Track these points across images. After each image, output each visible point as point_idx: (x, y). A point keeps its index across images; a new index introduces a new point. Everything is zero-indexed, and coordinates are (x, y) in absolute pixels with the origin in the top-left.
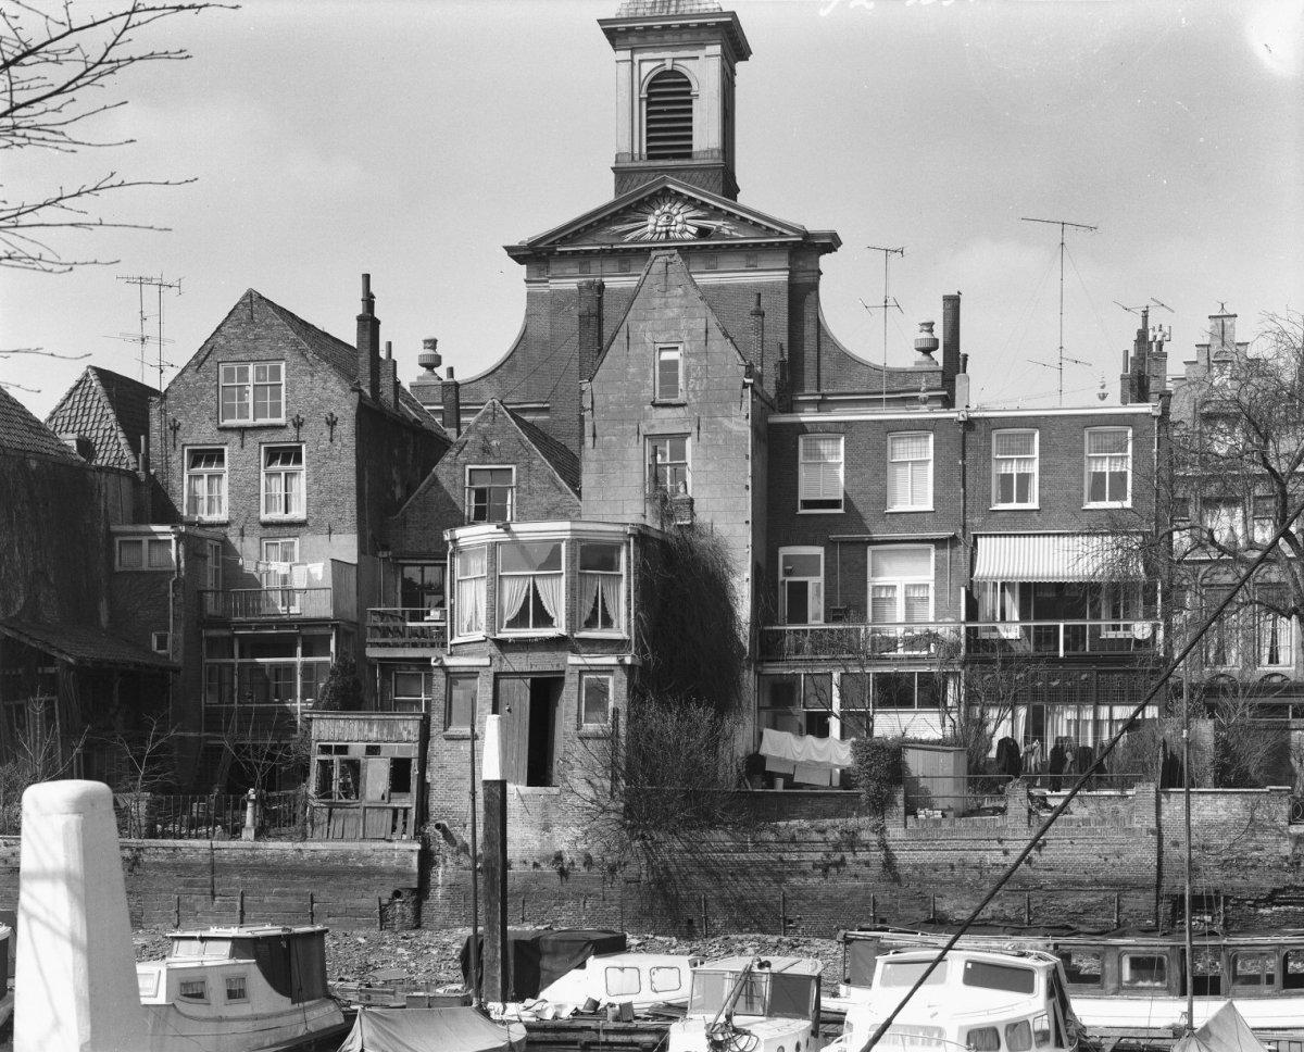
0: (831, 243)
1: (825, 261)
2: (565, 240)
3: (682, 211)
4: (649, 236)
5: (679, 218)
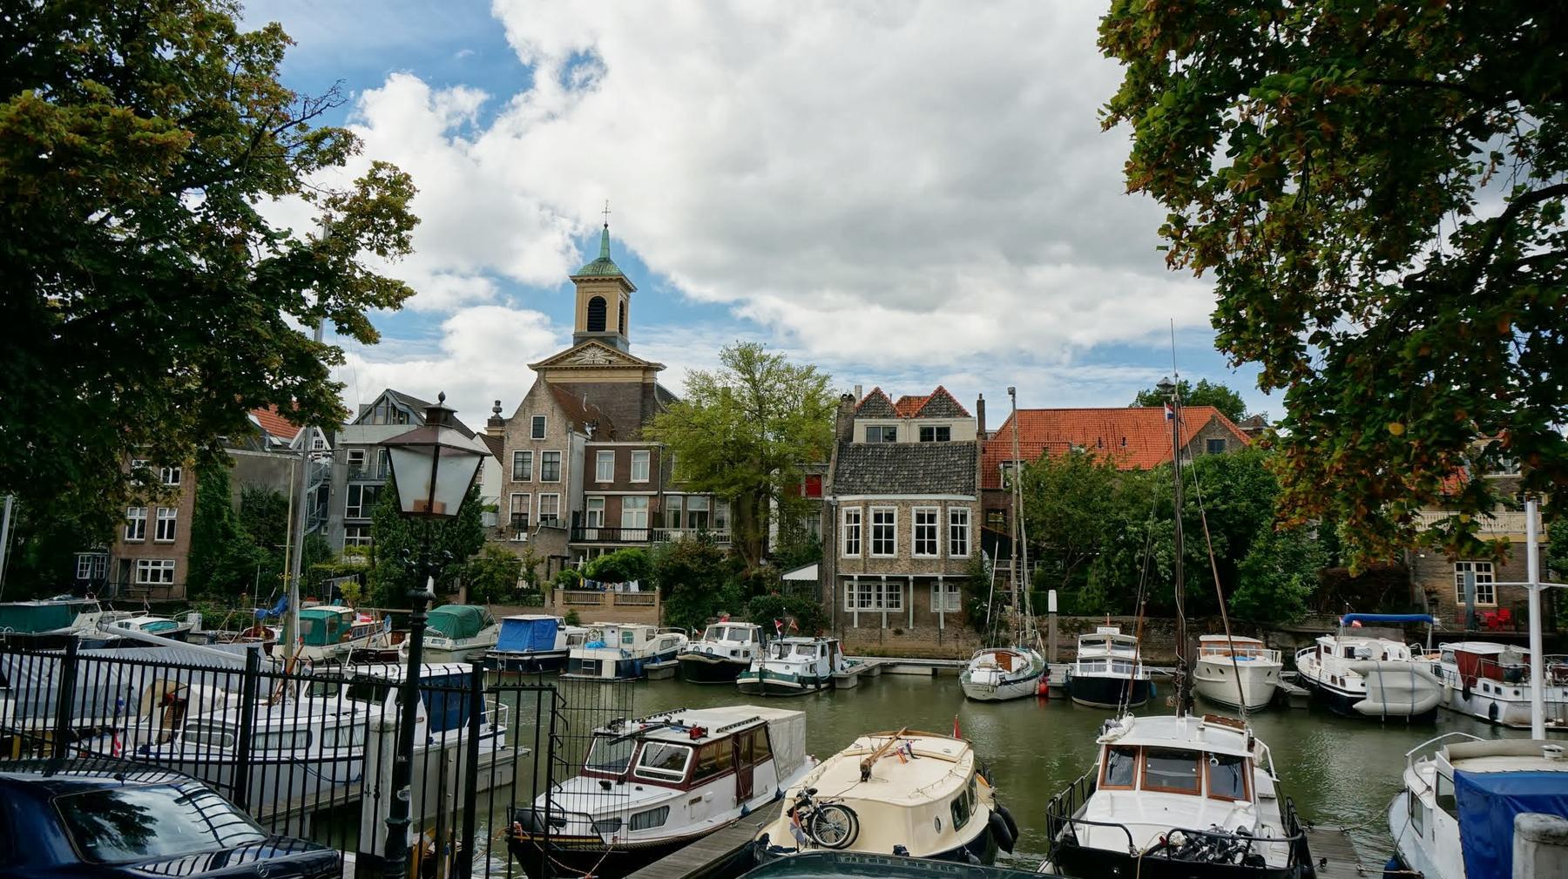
0: (658, 368)
1: (659, 374)
2: (552, 363)
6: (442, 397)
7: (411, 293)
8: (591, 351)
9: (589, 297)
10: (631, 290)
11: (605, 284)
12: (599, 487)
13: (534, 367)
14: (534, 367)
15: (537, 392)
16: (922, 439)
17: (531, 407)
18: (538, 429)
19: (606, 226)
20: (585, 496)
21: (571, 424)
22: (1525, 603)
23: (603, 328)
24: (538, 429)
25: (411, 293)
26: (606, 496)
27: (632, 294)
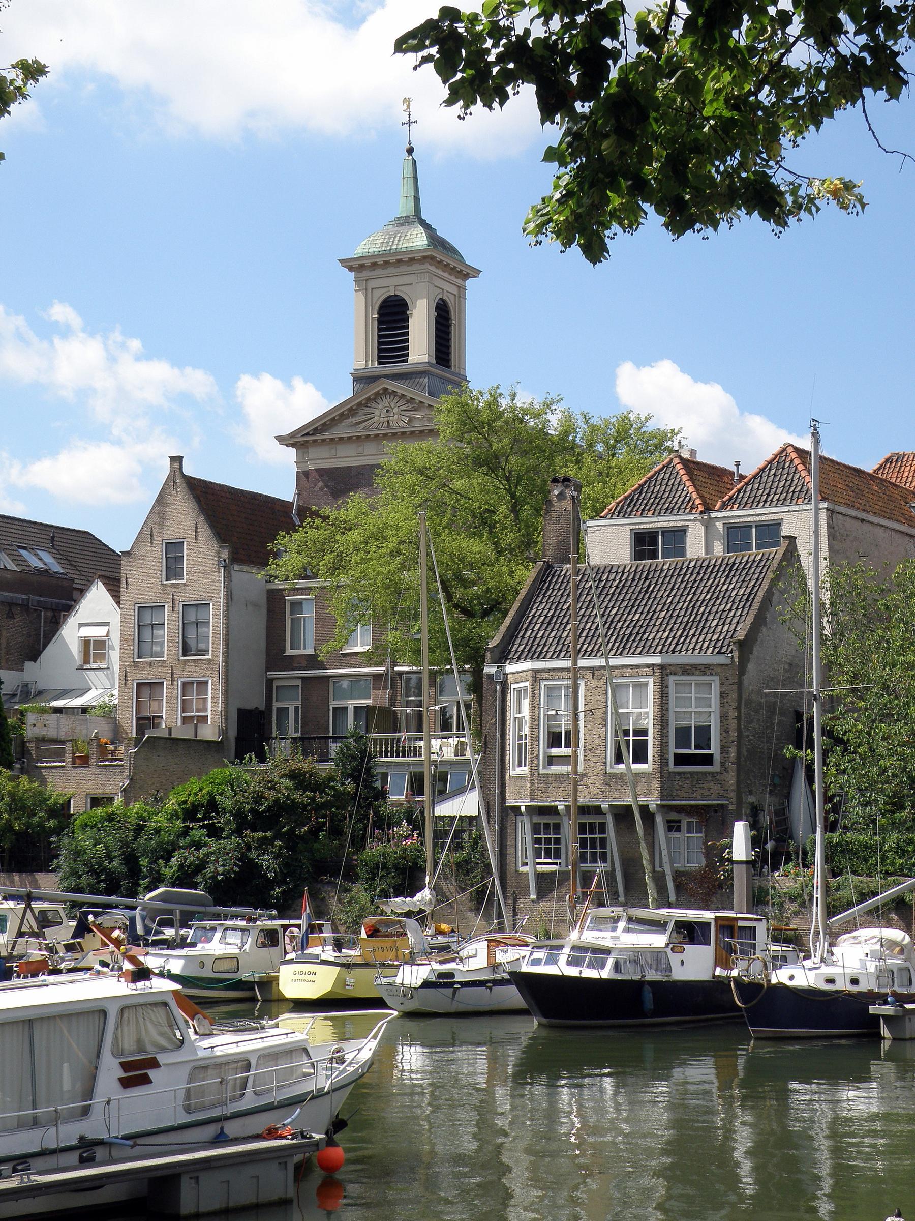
2: (316, 431)
3: (398, 405)
4: (375, 425)
5: (395, 410)
6: (738, 464)
7: (716, 230)
8: (384, 403)
9: (380, 296)
10: (467, 276)
11: (403, 269)
12: (291, 663)
13: (287, 440)
14: (287, 440)
15: (169, 499)
16: (638, 555)
17: (162, 525)
18: (173, 566)
19: (410, 151)
20: (270, 682)
21: (225, 554)
22: (561, 733)
23: (404, 358)
24: (173, 566)
25: (716, 230)
26: (304, 679)
27: (470, 283)
